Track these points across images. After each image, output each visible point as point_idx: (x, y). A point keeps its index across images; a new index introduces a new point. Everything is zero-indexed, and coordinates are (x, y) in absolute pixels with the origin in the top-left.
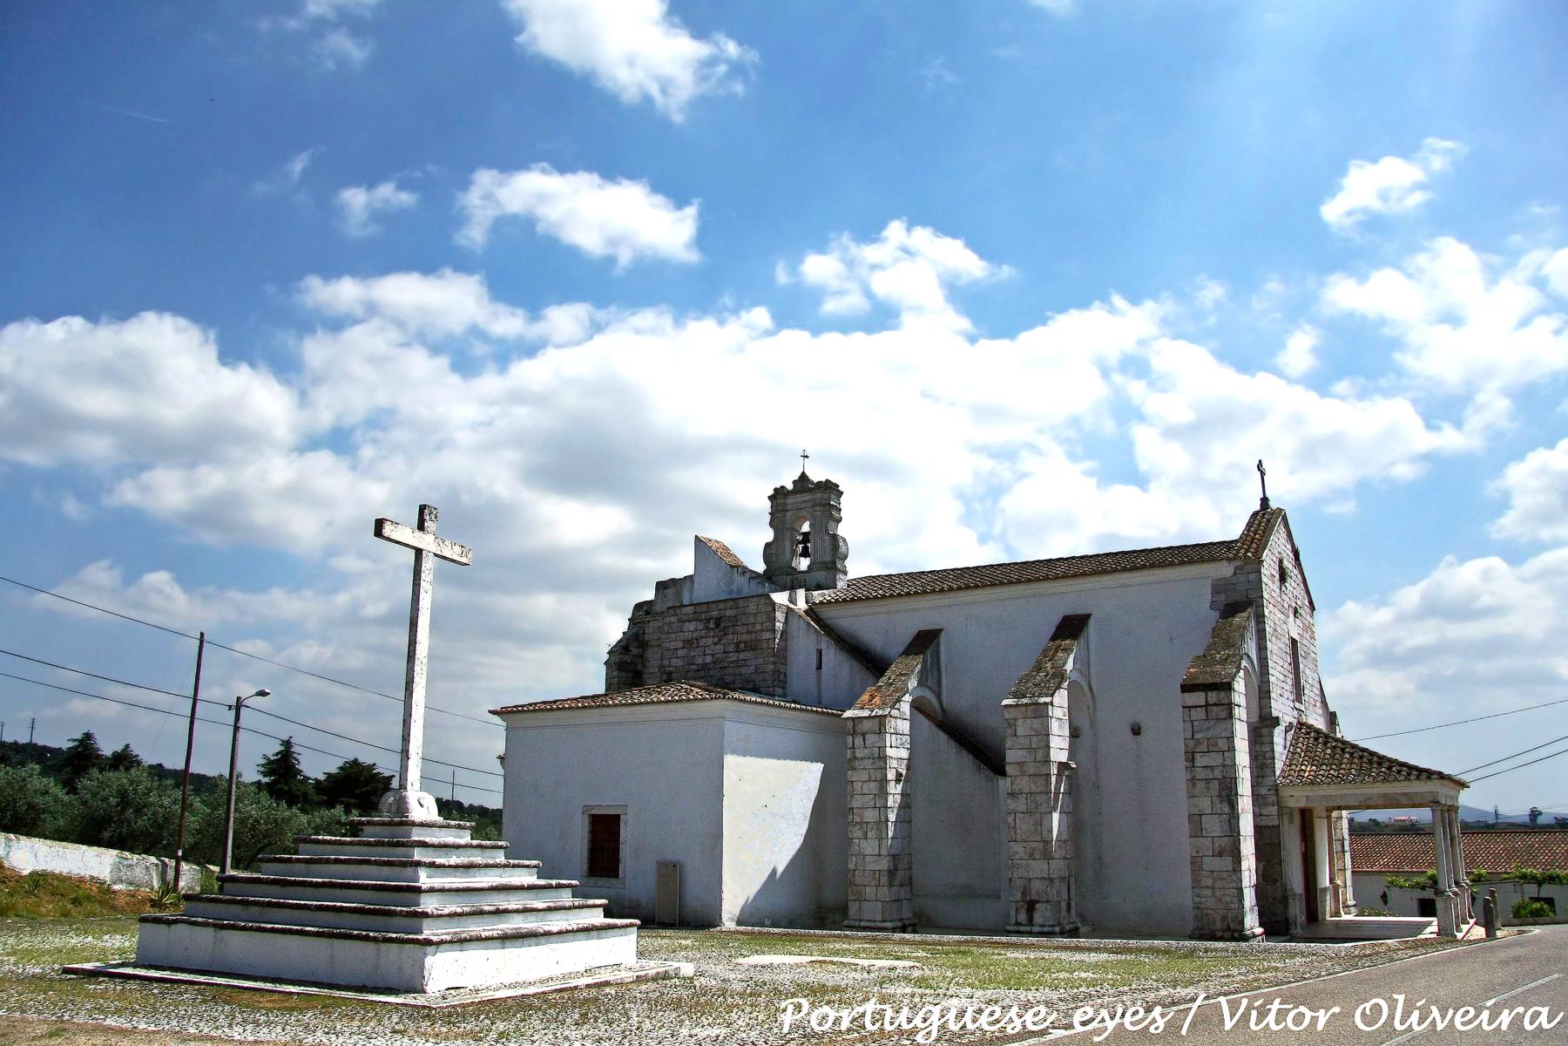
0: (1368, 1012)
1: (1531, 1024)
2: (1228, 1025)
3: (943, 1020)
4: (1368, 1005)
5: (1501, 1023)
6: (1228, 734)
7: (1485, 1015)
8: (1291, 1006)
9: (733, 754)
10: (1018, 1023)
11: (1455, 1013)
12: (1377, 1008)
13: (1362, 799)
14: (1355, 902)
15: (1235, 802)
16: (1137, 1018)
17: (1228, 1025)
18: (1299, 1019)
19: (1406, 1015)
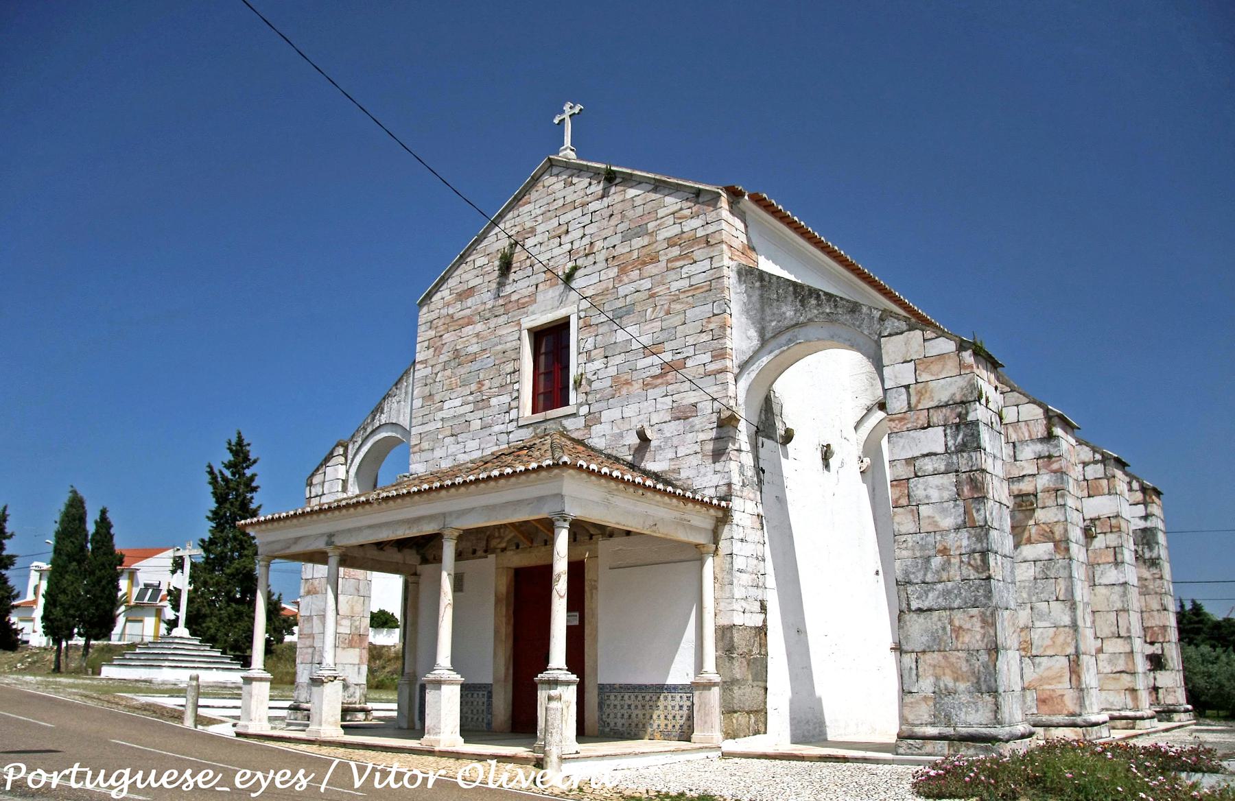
2: (357, 784)
10: (191, 782)
11: (275, 774)
17: (357, 784)
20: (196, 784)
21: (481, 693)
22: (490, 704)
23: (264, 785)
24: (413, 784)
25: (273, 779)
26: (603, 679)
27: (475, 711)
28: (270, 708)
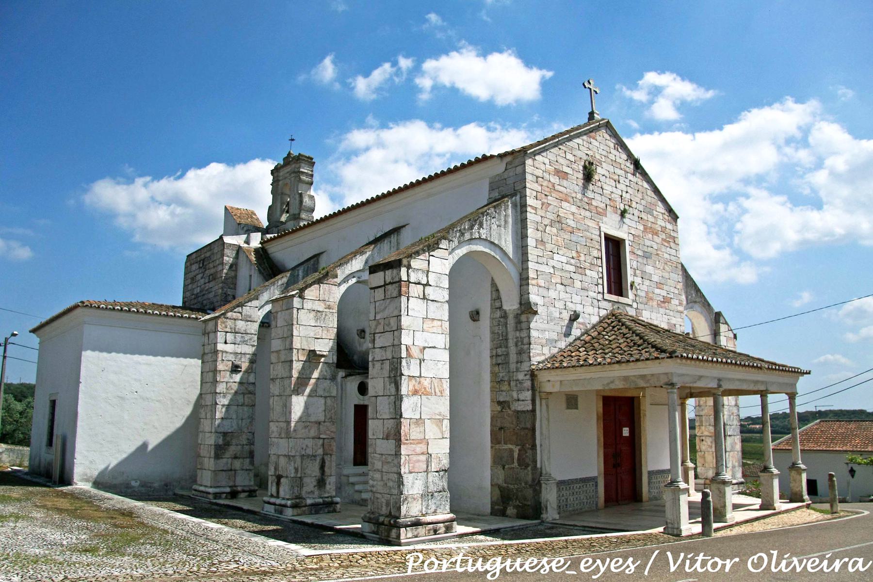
0: (755, 561)
1: (853, 568)
2: (673, 569)
3: (503, 565)
4: (756, 557)
5: (834, 568)
6: (396, 313)
7: (825, 563)
8: (710, 558)
9: (93, 350)
10: (547, 567)
11: (611, 561)
12: (761, 558)
13: (606, 382)
14: (743, 480)
15: (399, 384)
16: (618, 565)
17: (673, 569)
18: (715, 565)
19: (778, 564)
20: (551, 568)
21: (591, 483)
22: (597, 492)
23: (602, 570)
24: (714, 569)
25: (806, 565)
26: (650, 469)
27: (588, 497)
28: (690, 523)
